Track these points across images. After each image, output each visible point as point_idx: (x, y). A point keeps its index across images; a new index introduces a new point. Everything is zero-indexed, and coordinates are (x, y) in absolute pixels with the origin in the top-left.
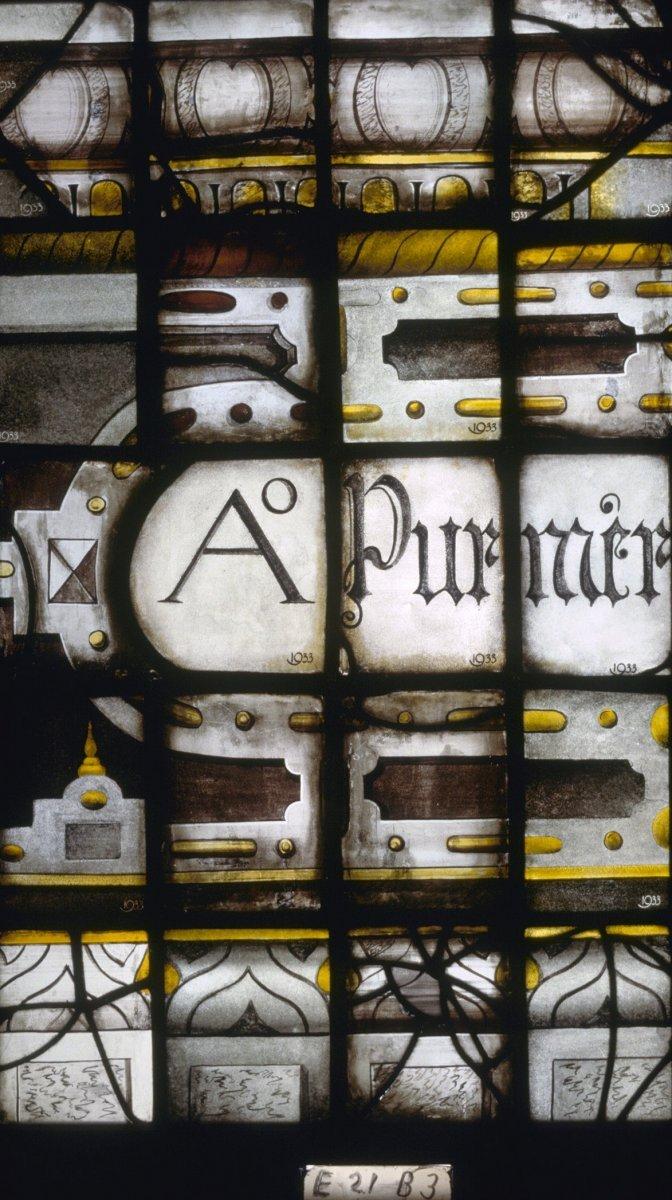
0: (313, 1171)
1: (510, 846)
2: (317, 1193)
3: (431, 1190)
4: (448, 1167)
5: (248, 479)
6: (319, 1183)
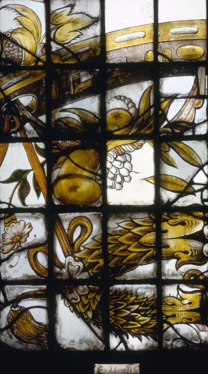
0: (97, 366)
2: (98, 372)
3: (135, 370)
6: (99, 370)
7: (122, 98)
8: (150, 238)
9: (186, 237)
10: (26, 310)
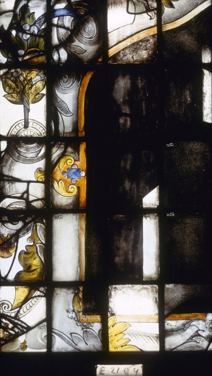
2: (100, 373)
4: (141, 365)
6: (101, 371)
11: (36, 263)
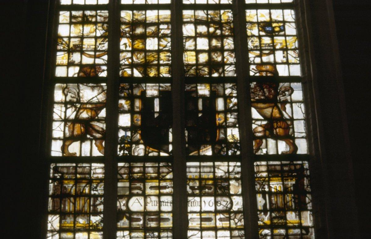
1: (159, 224)
5: (138, 198)
7: (150, 220)
8: (156, 56)
9: (165, 56)
10: (125, 71)
11: (228, 101)
